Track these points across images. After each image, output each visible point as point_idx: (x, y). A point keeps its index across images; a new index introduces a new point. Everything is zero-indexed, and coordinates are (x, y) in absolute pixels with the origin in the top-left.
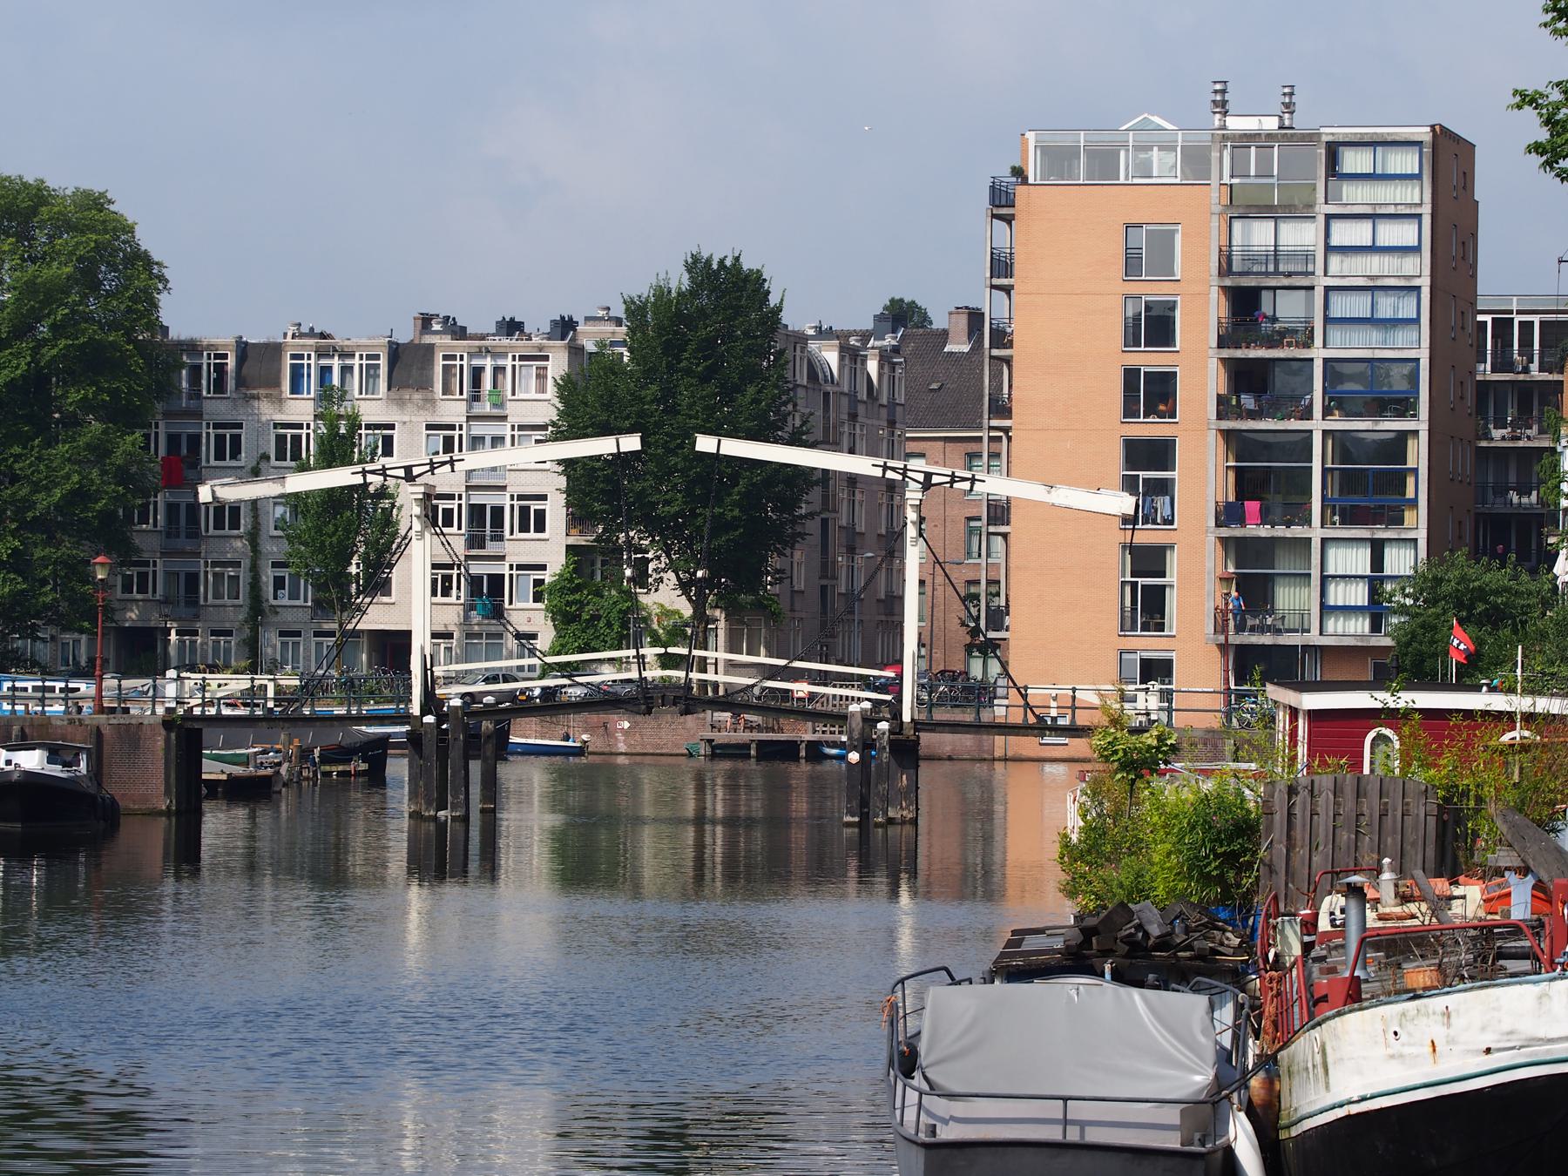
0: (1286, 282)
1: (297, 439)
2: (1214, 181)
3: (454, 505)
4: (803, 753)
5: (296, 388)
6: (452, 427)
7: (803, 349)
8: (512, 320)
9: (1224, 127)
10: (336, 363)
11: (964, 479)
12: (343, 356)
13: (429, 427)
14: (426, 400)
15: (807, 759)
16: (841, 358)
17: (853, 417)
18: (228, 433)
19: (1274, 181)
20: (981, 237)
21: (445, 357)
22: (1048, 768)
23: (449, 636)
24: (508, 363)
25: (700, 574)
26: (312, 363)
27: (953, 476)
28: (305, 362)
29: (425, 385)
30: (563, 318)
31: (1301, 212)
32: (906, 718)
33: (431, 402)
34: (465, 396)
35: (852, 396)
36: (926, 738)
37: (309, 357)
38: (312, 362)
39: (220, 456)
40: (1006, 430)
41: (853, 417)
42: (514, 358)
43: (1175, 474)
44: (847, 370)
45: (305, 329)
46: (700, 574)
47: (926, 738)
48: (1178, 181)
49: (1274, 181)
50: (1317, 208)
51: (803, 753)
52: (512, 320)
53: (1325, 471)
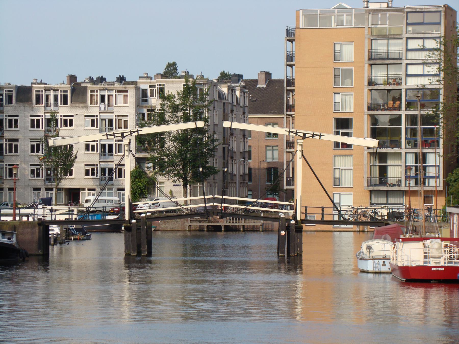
0: (391, 61)
1: (38, 121)
2: (366, 28)
3: (95, 144)
4: (223, 229)
5: (38, 102)
6: (94, 116)
7: (216, 87)
8: (102, 77)
9: (367, 7)
10: (52, 94)
11: (317, 135)
12: (54, 90)
13: (86, 116)
14: (30, 106)
15: (224, 231)
16: (228, 90)
17: (232, 111)
18: (13, 118)
19: (387, 26)
20: (282, 47)
21: (91, 91)
22: (335, 233)
23: (94, 190)
24: (113, 93)
25: (201, 169)
26: (44, 94)
27: (313, 134)
28: (41, 93)
29: (85, 101)
30: (120, 76)
31: (398, 37)
32: (299, 219)
33: (86, 107)
34: (43, 105)
35: (232, 104)
36: (304, 225)
37: (42, 91)
38: (43, 93)
39: (10, 126)
40: (291, 115)
41: (232, 111)
42: (116, 92)
43: (352, 130)
44: (230, 94)
45: (39, 81)
46: (201, 169)
47: (304, 225)
48: (353, 27)
49: (387, 26)
50: (403, 36)
51: (223, 229)
52: (102, 77)
53: (406, 129)
